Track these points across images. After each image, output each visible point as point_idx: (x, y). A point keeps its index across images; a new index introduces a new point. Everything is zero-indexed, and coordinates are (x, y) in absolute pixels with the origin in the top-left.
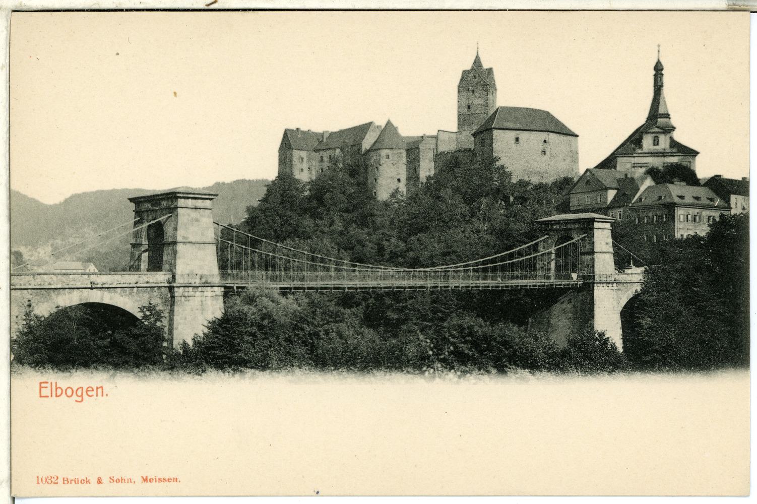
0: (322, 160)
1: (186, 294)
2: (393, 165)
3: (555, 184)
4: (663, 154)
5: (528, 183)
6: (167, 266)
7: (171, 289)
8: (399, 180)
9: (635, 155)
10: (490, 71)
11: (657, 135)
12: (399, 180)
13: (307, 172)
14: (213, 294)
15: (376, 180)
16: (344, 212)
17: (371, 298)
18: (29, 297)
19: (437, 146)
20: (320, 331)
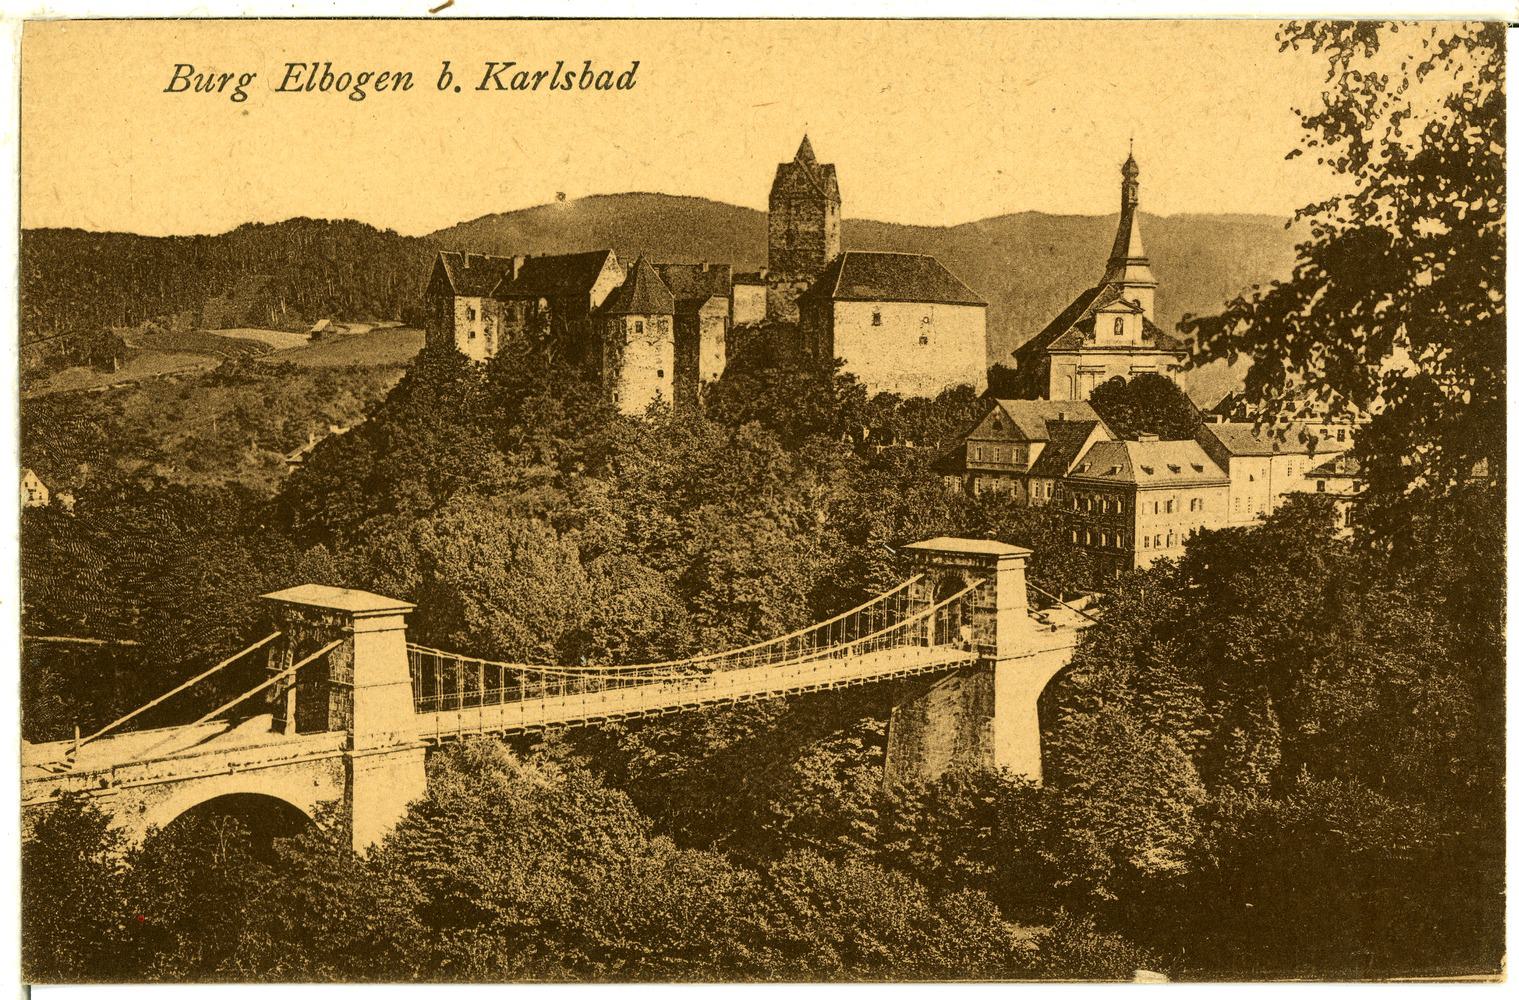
2: (650, 344)
4: (1131, 350)
5: (896, 398)
6: (333, 721)
8: (661, 374)
9: (1081, 352)
10: (830, 169)
12: (661, 374)
13: (484, 338)
16: (558, 435)
18: (143, 797)
19: (731, 312)
20: (583, 829)
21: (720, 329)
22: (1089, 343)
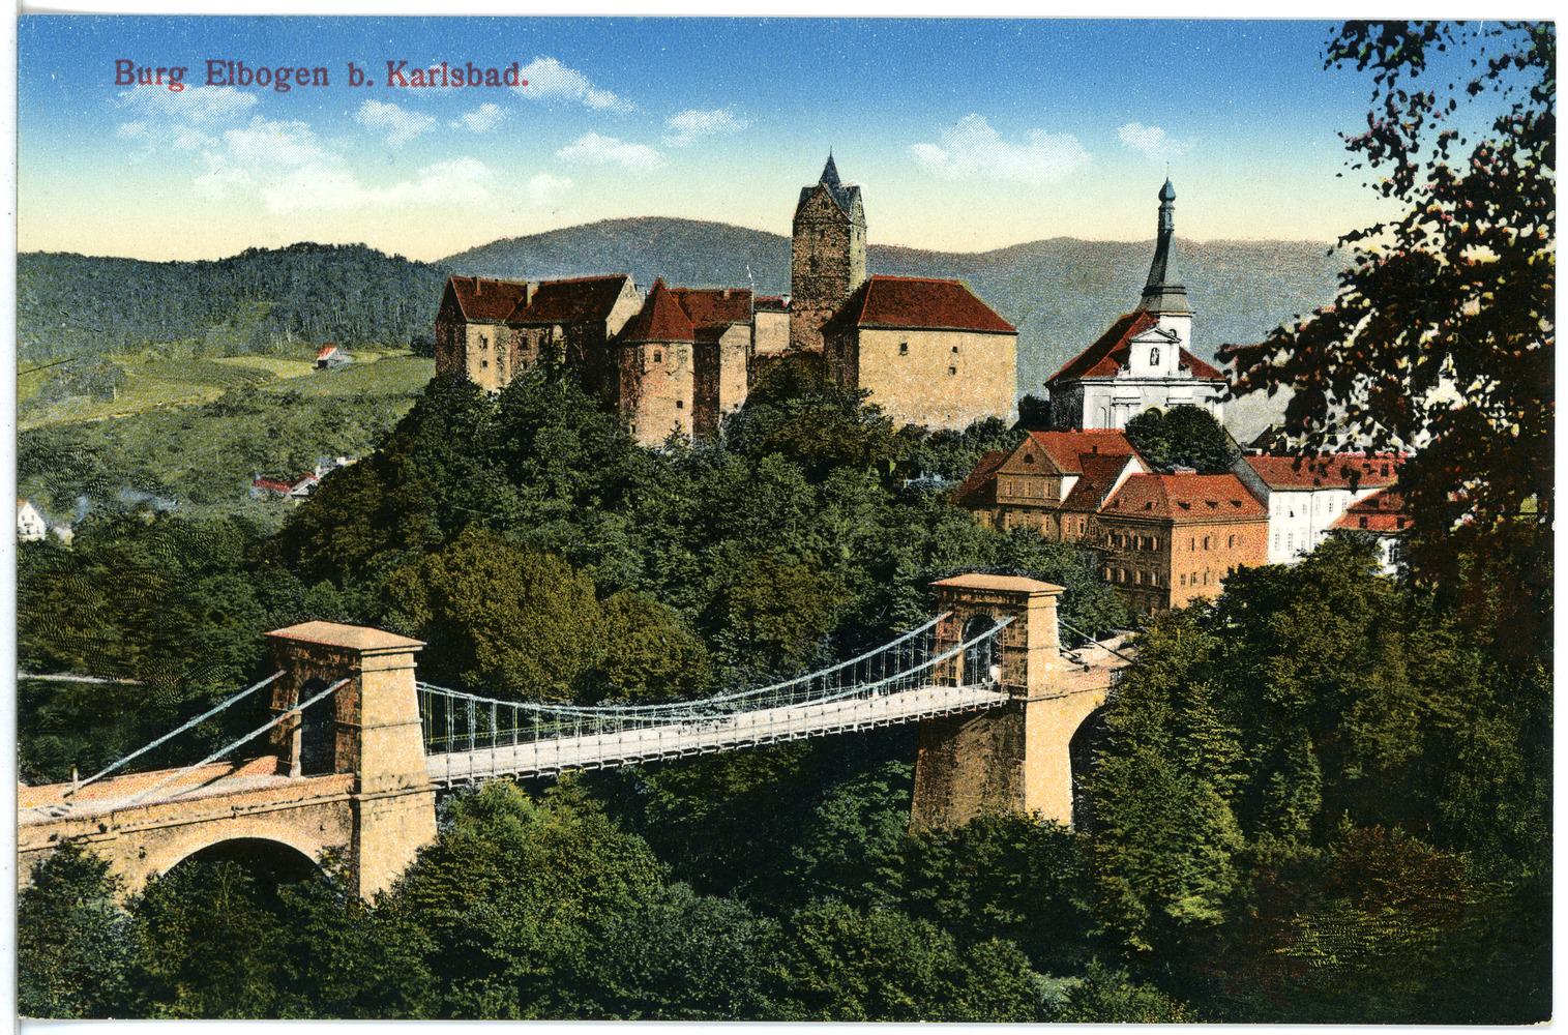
0: (524, 345)
1: (378, 810)
3: (971, 429)
4: (1167, 382)
5: (923, 431)
7: (355, 804)
10: (854, 191)
11: (1156, 345)
12: (680, 404)
14: (420, 804)
15: (635, 402)
16: (576, 467)
17: (641, 681)
19: (753, 341)
20: (598, 875)
21: (742, 357)
22: (1123, 374)
